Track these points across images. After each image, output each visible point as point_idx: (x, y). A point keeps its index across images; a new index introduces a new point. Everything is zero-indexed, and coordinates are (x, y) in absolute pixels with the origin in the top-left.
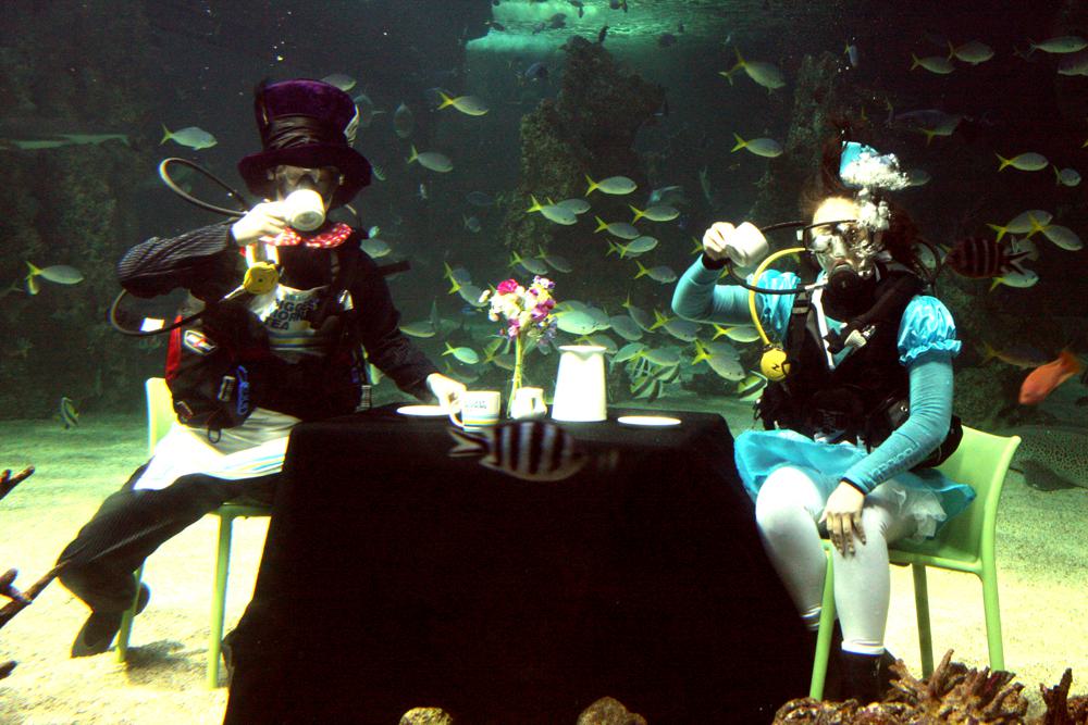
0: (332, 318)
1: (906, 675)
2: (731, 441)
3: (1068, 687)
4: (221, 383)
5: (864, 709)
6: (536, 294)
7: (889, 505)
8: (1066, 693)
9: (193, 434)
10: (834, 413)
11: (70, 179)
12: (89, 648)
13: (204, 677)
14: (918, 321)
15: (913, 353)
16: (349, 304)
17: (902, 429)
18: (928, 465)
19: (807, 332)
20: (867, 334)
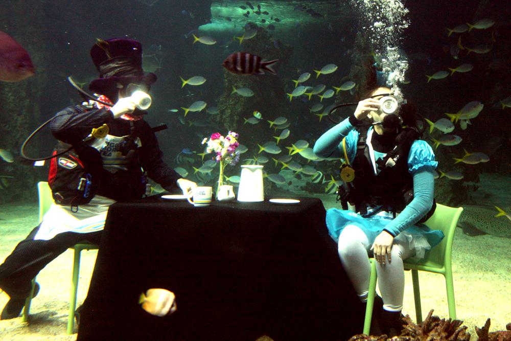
0: (132, 151)
1: (411, 322)
2: (325, 212)
3: (488, 327)
4: (79, 182)
5: (390, 340)
6: (230, 140)
7: (405, 243)
8: (488, 330)
9: (64, 210)
10: (376, 197)
11: (7, 89)
12: (10, 315)
13: (66, 329)
14: (418, 152)
15: (416, 167)
16: (140, 145)
17: (411, 204)
18: (420, 223)
19: (365, 157)
20: (395, 159)
